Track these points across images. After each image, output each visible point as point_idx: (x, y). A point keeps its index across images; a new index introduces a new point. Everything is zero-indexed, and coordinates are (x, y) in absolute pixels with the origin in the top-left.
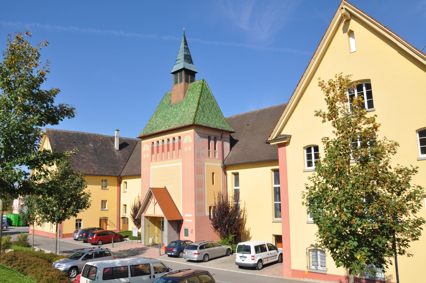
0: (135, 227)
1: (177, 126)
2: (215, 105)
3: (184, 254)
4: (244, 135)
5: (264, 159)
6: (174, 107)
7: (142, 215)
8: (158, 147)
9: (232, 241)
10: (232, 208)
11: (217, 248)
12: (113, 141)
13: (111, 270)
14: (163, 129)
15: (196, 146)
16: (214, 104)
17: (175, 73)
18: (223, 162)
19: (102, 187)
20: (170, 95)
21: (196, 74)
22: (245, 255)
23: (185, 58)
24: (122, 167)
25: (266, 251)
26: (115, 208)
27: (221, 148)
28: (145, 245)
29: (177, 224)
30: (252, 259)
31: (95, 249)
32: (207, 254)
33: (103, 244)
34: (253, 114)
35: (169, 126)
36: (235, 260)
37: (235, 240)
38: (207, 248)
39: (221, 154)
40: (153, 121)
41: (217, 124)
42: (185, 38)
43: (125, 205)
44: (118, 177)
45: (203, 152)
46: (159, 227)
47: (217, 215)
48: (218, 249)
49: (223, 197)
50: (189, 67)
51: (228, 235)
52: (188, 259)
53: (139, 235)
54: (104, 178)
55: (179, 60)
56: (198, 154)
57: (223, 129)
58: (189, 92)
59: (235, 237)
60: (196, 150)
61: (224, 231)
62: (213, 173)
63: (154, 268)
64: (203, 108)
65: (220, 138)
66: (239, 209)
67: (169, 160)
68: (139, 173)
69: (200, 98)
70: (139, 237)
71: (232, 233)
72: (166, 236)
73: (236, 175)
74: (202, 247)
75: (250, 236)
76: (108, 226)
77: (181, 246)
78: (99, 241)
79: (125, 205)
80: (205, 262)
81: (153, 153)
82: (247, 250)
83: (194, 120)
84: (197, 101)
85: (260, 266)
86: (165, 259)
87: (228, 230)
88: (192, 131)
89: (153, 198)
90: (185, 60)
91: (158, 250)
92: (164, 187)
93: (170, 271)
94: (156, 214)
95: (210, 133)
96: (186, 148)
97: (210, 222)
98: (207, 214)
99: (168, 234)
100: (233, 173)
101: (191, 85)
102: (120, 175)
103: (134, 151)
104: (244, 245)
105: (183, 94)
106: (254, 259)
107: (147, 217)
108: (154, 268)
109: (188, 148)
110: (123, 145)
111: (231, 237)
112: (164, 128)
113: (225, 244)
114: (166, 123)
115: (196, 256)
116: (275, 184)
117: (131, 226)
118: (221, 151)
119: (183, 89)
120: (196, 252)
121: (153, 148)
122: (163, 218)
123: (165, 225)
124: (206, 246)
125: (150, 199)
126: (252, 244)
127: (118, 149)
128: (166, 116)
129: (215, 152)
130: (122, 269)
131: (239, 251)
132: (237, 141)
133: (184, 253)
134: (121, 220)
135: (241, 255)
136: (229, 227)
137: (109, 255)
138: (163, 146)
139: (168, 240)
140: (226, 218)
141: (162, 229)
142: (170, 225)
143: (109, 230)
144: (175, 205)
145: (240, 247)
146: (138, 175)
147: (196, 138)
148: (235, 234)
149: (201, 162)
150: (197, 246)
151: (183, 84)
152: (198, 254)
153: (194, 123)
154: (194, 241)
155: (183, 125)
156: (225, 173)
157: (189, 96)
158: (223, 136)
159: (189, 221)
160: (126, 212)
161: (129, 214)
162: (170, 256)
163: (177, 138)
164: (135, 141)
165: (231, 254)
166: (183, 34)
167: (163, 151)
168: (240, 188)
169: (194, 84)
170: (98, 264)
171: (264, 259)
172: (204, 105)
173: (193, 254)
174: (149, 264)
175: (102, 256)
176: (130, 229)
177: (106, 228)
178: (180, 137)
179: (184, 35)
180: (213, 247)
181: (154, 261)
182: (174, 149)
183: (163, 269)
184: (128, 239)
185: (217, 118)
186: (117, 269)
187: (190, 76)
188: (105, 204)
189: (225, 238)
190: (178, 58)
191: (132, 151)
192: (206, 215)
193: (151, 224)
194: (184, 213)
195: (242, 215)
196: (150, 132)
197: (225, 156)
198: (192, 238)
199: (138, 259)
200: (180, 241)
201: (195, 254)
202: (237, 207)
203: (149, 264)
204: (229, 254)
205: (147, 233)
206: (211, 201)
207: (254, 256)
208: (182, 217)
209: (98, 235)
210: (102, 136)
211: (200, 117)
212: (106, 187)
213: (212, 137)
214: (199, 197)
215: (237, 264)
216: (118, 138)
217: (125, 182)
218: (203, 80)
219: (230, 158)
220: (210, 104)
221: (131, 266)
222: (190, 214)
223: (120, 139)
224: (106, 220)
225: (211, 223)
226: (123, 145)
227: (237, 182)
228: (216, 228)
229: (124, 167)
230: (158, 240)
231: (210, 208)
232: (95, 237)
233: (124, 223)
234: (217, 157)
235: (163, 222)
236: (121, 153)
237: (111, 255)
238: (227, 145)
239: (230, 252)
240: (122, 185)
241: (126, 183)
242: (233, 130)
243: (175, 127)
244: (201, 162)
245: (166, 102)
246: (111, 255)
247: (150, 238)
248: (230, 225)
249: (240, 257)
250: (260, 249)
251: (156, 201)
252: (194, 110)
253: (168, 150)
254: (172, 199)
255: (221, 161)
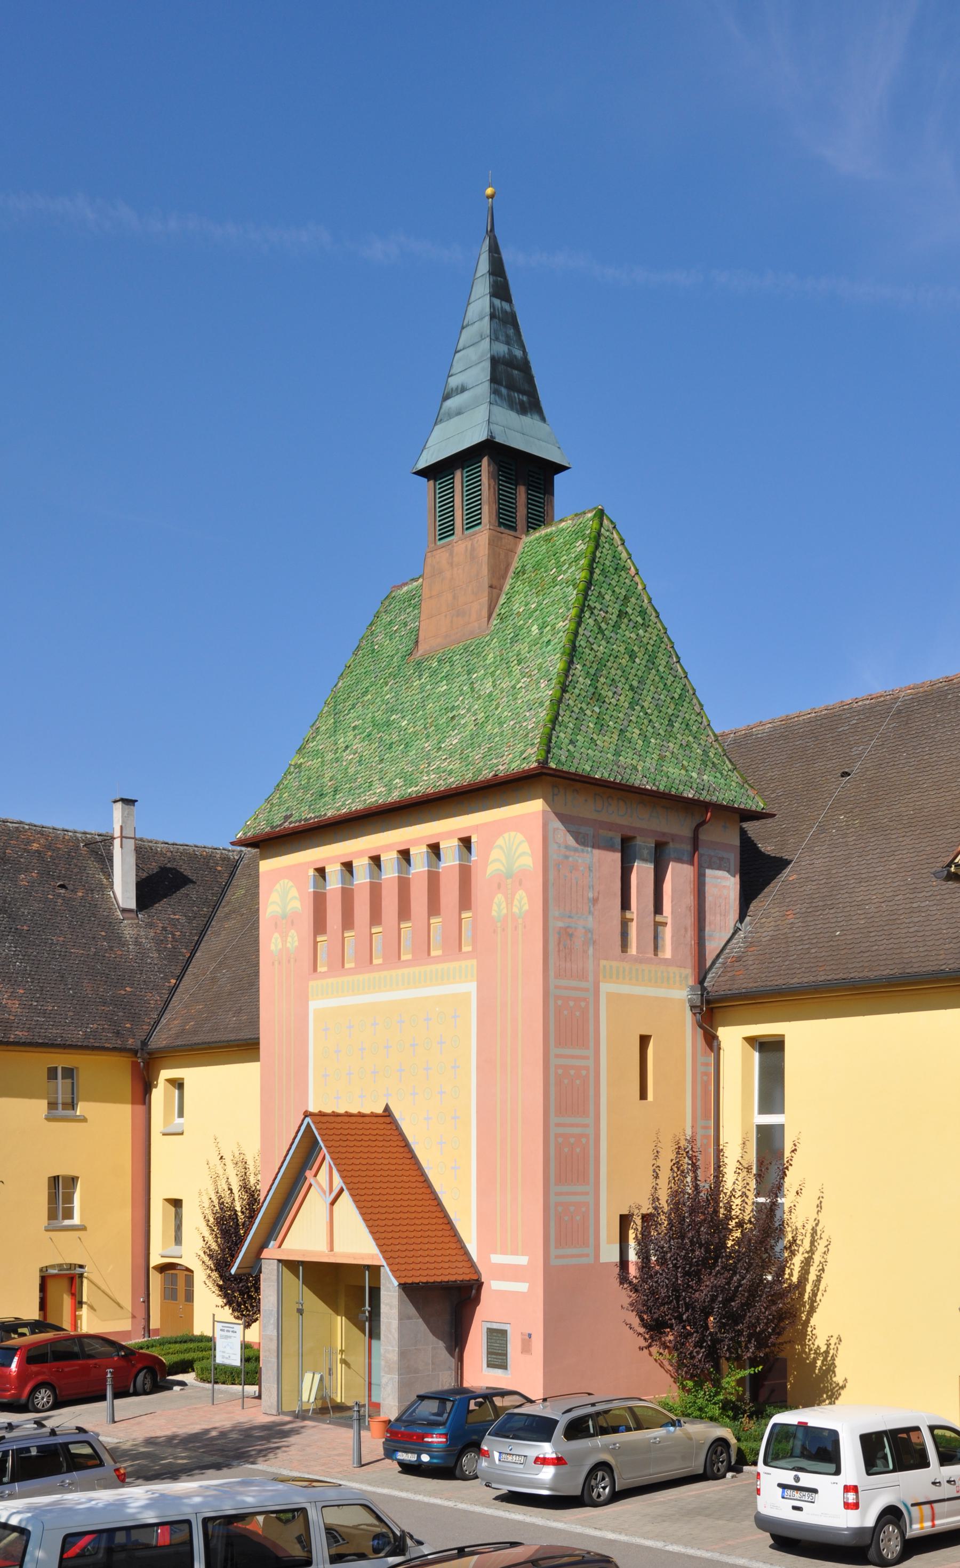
0: (226, 1314)
1: (453, 781)
2: (662, 661)
3: (484, 1463)
4: (822, 829)
5: (931, 966)
6: (434, 673)
7: (266, 1253)
8: (347, 895)
9: (740, 1398)
10: (740, 1225)
11: (659, 1432)
12: (106, 861)
13: (103, 1544)
14: (378, 795)
15: (554, 888)
16: (659, 655)
17: (437, 472)
18: (701, 981)
19: (52, 1105)
20: (414, 601)
21: (558, 479)
22: (807, 1480)
23: (494, 380)
24: (154, 999)
25: (923, 1463)
26: (124, 1216)
27: (689, 900)
28: (280, 1412)
29: (450, 1303)
30: (847, 1506)
31: (15, 1433)
32: (603, 1466)
33: (58, 1404)
34: (877, 710)
35: (409, 780)
36: (755, 1503)
37: (754, 1397)
38: (604, 1431)
39: (690, 936)
40: (318, 754)
41: (673, 771)
42: (494, 250)
43: (177, 1203)
44: (134, 1052)
45: (590, 922)
46: (354, 1319)
47: (662, 1261)
48: (663, 1439)
49: (696, 1159)
50: (523, 434)
51: (717, 1368)
52: (505, 1489)
53: (251, 1356)
54: (61, 1060)
55: (463, 389)
56: (567, 934)
57: (705, 796)
58: (519, 586)
59: (753, 1377)
60: (554, 912)
61: (699, 1344)
62: (644, 1040)
63: (332, 1533)
64: (595, 678)
65: (688, 847)
66: (781, 1231)
67: (408, 964)
68: (245, 1035)
69: (579, 620)
70: (250, 1369)
71: (738, 1358)
72: (390, 1365)
73: (770, 1048)
74: (576, 1429)
75: (838, 1379)
76: (84, 1312)
77: (471, 1418)
78: (36, 1388)
79: (177, 1203)
80: (595, 1505)
81: (319, 925)
82: (821, 1450)
83: (548, 745)
84: (562, 639)
85: (891, 1546)
86: (382, 1483)
87: (716, 1341)
88: (535, 807)
89: (325, 1168)
90: (495, 392)
91: (346, 1435)
92: (379, 1110)
93: (414, 1551)
94: (336, 1249)
95: (629, 819)
96: (499, 898)
97: (624, 1297)
98: (610, 1254)
99: (403, 1354)
100: (750, 1040)
101: (530, 543)
102: (144, 1043)
103: (221, 913)
104: (803, 1426)
105: (484, 600)
106: (856, 1506)
107: (291, 1265)
108: (332, 1533)
109: (510, 902)
110: (162, 880)
111: (732, 1380)
112: (379, 789)
113: (701, 1415)
114: (393, 761)
115: (548, 1473)
116: (779, 1130)
117: (209, 1311)
118: (689, 921)
119: (485, 571)
120: (547, 1449)
121: (319, 901)
122: (375, 1270)
123: (384, 1309)
124: (602, 1422)
125: (309, 1174)
126: (846, 1419)
127: (132, 905)
128: (388, 724)
129: (657, 925)
130: (162, 1537)
131: (776, 1457)
132: (780, 864)
133: (486, 1454)
134: (156, 1280)
135: (787, 1477)
136: (721, 1326)
137: (93, 1461)
138: (375, 890)
139: (403, 1386)
140: (709, 1281)
141: (370, 1325)
142: (412, 1310)
143: (92, 1332)
144: (439, 1204)
145: (783, 1433)
146: (246, 1047)
147: (553, 847)
148: (753, 1362)
149: (583, 976)
150: (555, 1423)
151: (482, 536)
152: (558, 1461)
153: (543, 764)
154: (536, 1393)
155: (487, 774)
156: (711, 1041)
157: (517, 607)
158: (703, 837)
159: (512, 1290)
160: (178, 1240)
161: (195, 1248)
162: (408, 1469)
163: (449, 847)
164: (225, 859)
165: (730, 1469)
166: (483, 225)
167: (376, 917)
168: (792, 1121)
169: (548, 539)
170: (38, 1513)
171: (915, 1510)
172: (602, 663)
173: (533, 1464)
174: (304, 1510)
175: (55, 1470)
176: (201, 1327)
177: (75, 1320)
178: (466, 843)
179: (491, 233)
180: (639, 1427)
181: (331, 1495)
182: (434, 908)
183: (377, 1536)
184: (189, 1378)
185: (670, 735)
186: (135, 1535)
187: (522, 491)
188: (69, 1199)
189: (699, 1385)
190: (454, 382)
191: (210, 919)
192: (603, 1259)
193: (312, 1301)
194: (486, 1244)
195: (797, 1261)
196: (305, 814)
197: (713, 946)
198: (526, 1378)
199: (244, 1483)
200: (462, 1393)
201: (543, 1461)
202: (769, 1223)
203: (304, 1510)
204: (722, 1467)
205: (291, 1347)
206: (632, 1183)
207: (855, 1489)
208: (473, 1265)
209: (34, 1357)
210: (41, 831)
211: (577, 729)
212: (73, 1106)
213: (645, 844)
214: (568, 1165)
215: (763, 1522)
216: (130, 844)
217: (172, 1082)
218: (601, 514)
219: (739, 959)
220: (632, 656)
221: (206, 1521)
222: (515, 1253)
223: (143, 852)
224: (72, 1279)
225: (626, 1301)
226: (162, 880)
227: (772, 1091)
228: (655, 1328)
229: (167, 1003)
230: (348, 1387)
231: (625, 1221)
232: (14, 1367)
233: (170, 1294)
234: (667, 952)
235: (375, 1292)
236: (150, 925)
237: (101, 1464)
238: (725, 886)
239: (723, 1461)
240: (158, 1095)
241: (179, 1084)
242: (758, 804)
243: (442, 785)
244: (583, 976)
245: (389, 646)
246: (101, 1464)
247: (308, 1377)
248: (731, 1319)
249: (783, 1486)
250: (892, 1449)
251: (338, 1182)
252: (547, 692)
253: (404, 913)
254: (423, 1174)
255: (688, 975)
